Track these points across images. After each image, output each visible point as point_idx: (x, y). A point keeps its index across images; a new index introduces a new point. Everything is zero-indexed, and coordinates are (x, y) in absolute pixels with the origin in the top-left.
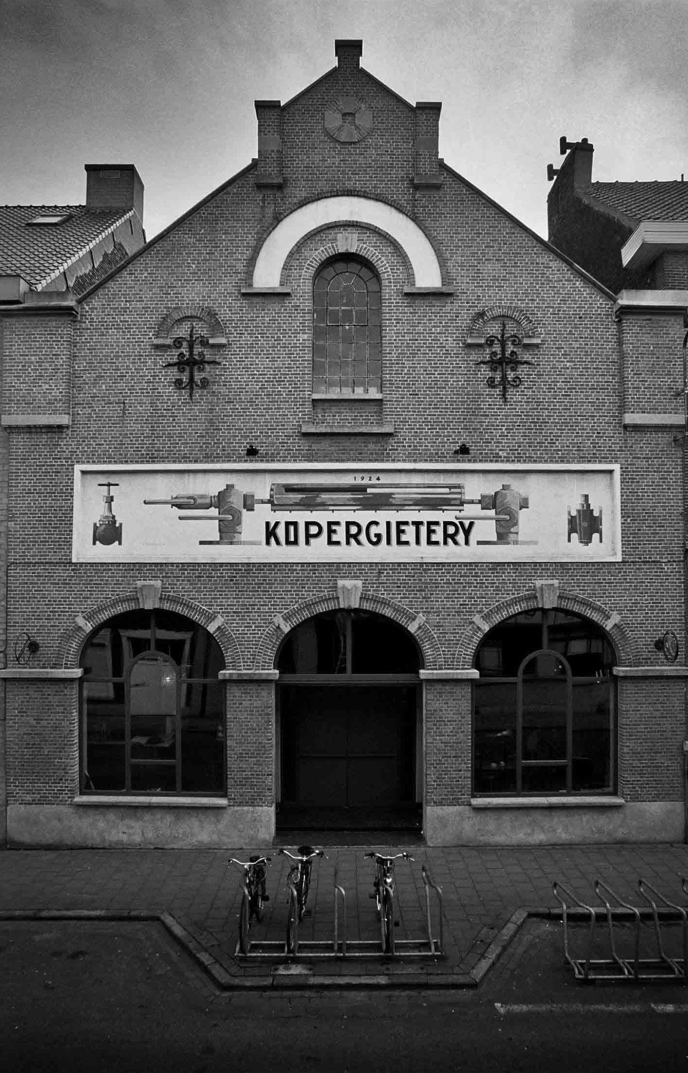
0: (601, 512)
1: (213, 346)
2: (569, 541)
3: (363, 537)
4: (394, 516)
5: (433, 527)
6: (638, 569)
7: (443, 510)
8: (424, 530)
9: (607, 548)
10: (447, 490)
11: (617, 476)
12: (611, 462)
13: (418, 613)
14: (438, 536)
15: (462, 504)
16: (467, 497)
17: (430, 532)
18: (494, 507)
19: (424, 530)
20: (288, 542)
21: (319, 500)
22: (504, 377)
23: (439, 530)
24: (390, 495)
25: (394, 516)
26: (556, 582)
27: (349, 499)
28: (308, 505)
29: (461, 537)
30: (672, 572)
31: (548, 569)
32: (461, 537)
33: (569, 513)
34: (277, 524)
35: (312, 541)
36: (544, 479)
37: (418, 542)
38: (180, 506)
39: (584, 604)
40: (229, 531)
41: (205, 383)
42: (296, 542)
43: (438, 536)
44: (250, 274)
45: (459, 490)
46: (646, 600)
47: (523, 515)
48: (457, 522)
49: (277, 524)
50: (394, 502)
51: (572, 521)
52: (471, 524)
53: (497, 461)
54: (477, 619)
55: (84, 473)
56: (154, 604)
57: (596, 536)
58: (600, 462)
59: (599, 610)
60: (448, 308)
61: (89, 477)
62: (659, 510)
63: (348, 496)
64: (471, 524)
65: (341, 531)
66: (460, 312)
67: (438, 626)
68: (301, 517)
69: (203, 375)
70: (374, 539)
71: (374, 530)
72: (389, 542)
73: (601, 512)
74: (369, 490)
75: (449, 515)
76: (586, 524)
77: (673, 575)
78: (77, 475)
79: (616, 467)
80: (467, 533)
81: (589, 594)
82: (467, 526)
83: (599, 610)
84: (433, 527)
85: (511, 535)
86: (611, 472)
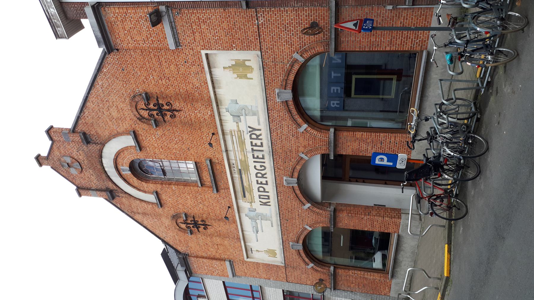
0: (232, 60)
1: (186, 217)
2: (252, 79)
3: (263, 172)
4: (251, 160)
5: (254, 144)
6: (264, 41)
7: (244, 139)
8: (255, 148)
9: (252, 58)
10: (234, 137)
11: (208, 52)
12: (201, 55)
13: (298, 155)
14: (258, 142)
15: (240, 131)
16: (236, 128)
17: (256, 145)
18: (239, 116)
19: (255, 148)
20: (269, 198)
21: (247, 186)
22: (168, 110)
23: (254, 142)
24: (241, 160)
25: (251, 160)
26: (277, 91)
27: (245, 176)
28: (251, 191)
29: (258, 133)
30: (264, 18)
31: (270, 93)
32: (258, 133)
33: (235, 78)
34: (260, 201)
35: (266, 190)
36: (219, 91)
37: (263, 151)
38: (257, 232)
39: (289, 74)
40: (264, 218)
41: (203, 221)
42: (268, 196)
43: (258, 142)
44: (153, 203)
45: (233, 132)
46: (284, 35)
47: (241, 103)
48: (249, 134)
49: (260, 201)
50: (243, 159)
51: (240, 77)
52: (249, 127)
53: (214, 116)
54: (302, 130)
55: (248, 257)
56: (289, 93)
57: (247, 63)
58: (202, 62)
59: (292, 66)
60: (140, 133)
61: (249, 256)
62: (225, 25)
63: (243, 176)
64: (249, 127)
65: (260, 180)
66: (141, 128)
67: (305, 147)
68: (256, 194)
69: (200, 221)
70: (263, 168)
71: (258, 167)
72: (264, 162)
73: (232, 60)
74: (240, 168)
75: (247, 137)
76: (240, 69)
77: (267, 17)
78: (249, 260)
79: (203, 52)
80: (255, 129)
81: (282, 71)
82: (251, 130)
83: (292, 66)
84: (254, 144)
85: (253, 109)
86: (207, 55)
